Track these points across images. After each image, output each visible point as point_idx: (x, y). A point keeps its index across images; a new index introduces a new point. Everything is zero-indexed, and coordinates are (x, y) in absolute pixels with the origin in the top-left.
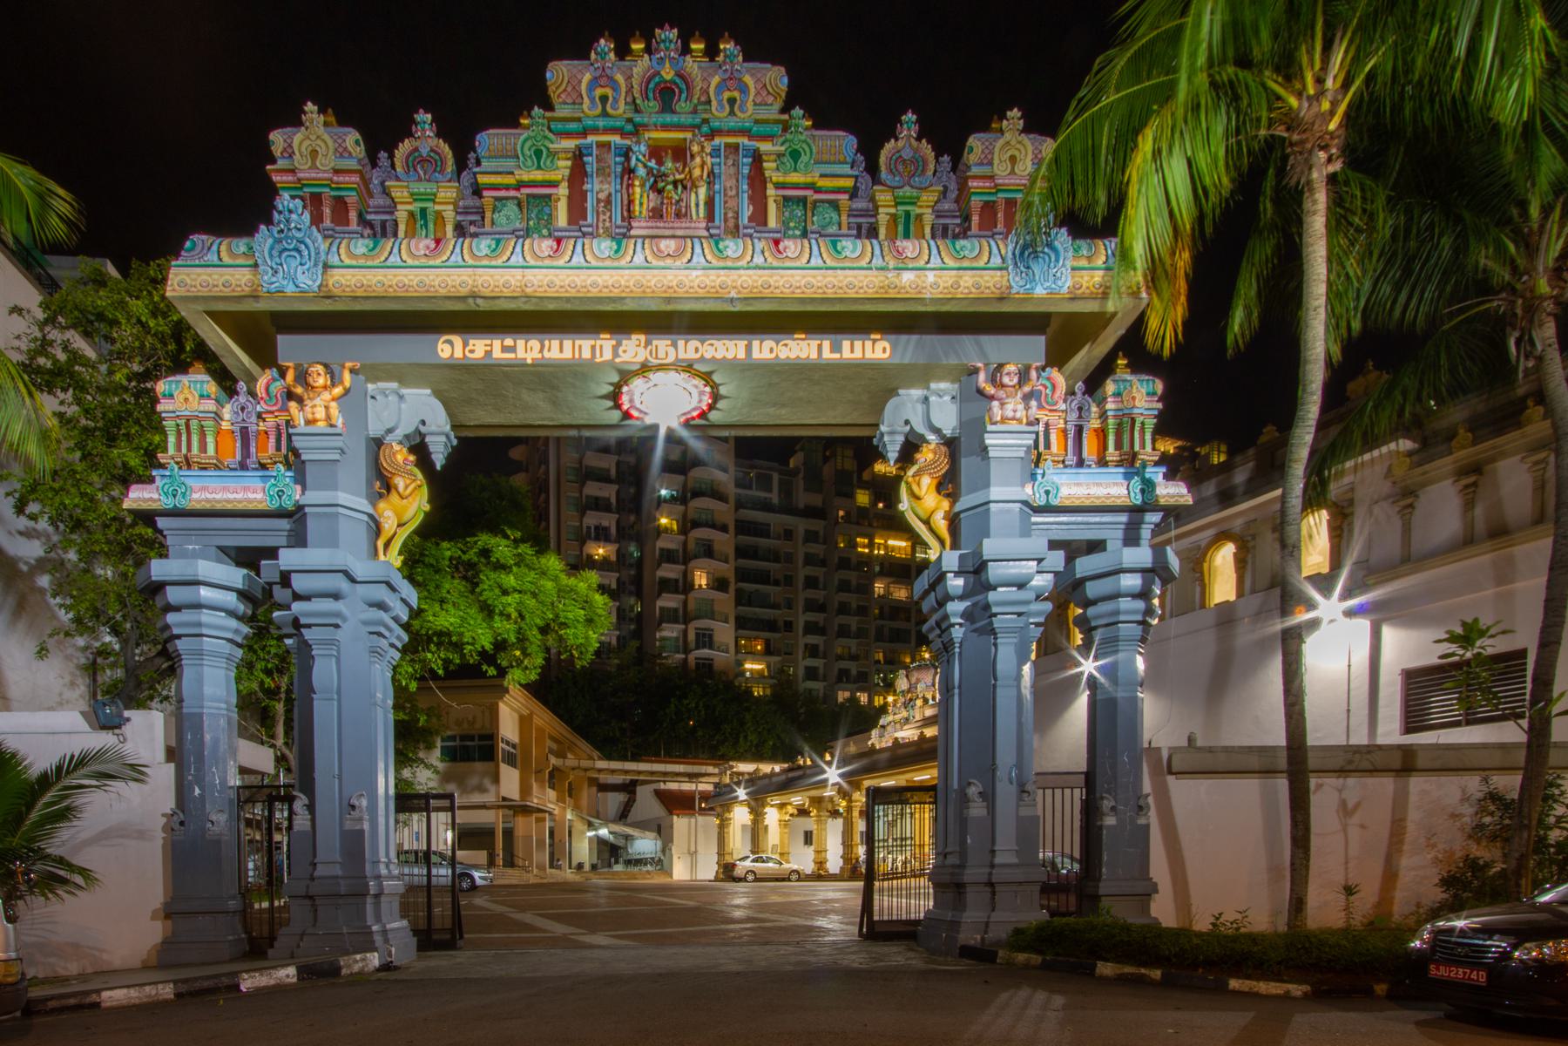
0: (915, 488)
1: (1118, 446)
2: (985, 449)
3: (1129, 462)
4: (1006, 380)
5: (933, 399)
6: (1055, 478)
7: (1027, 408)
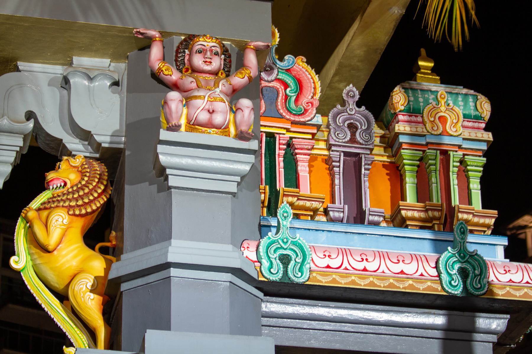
0: (39, 230)
1: (423, 193)
2: (162, 172)
3: (443, 223)
4: (198, 61)
5: (76, 81)
6: (299, 237)
7: (234, 109)
